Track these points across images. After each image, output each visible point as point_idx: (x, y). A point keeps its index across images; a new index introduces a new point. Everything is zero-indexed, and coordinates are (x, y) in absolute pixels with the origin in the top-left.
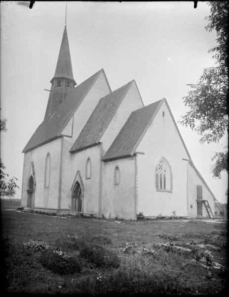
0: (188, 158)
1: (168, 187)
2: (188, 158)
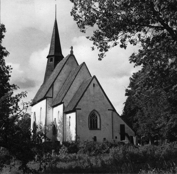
0: (112, 109)
1: (98, 127)
2: (112, 109)
